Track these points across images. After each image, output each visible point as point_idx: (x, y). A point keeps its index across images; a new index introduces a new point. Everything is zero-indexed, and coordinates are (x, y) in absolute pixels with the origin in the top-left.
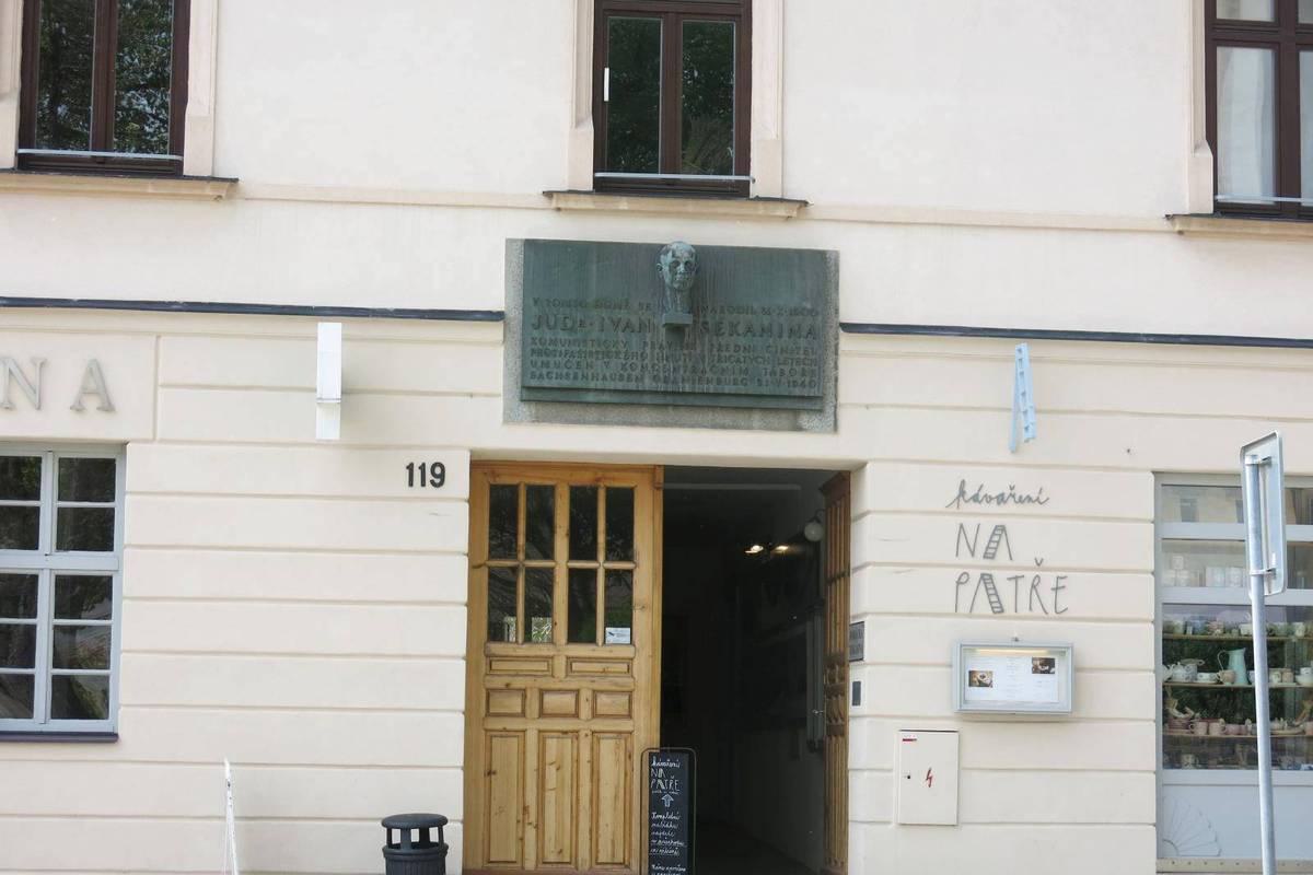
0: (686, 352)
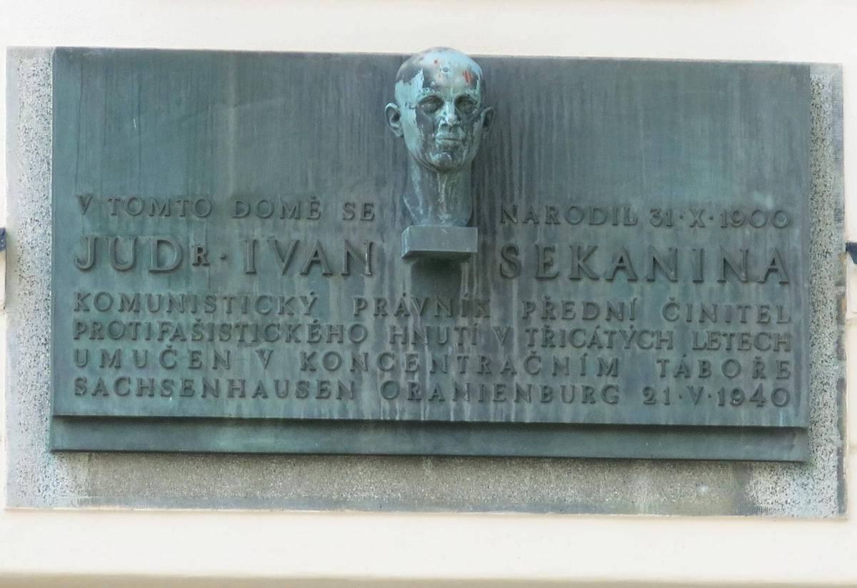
0: (463, 322)
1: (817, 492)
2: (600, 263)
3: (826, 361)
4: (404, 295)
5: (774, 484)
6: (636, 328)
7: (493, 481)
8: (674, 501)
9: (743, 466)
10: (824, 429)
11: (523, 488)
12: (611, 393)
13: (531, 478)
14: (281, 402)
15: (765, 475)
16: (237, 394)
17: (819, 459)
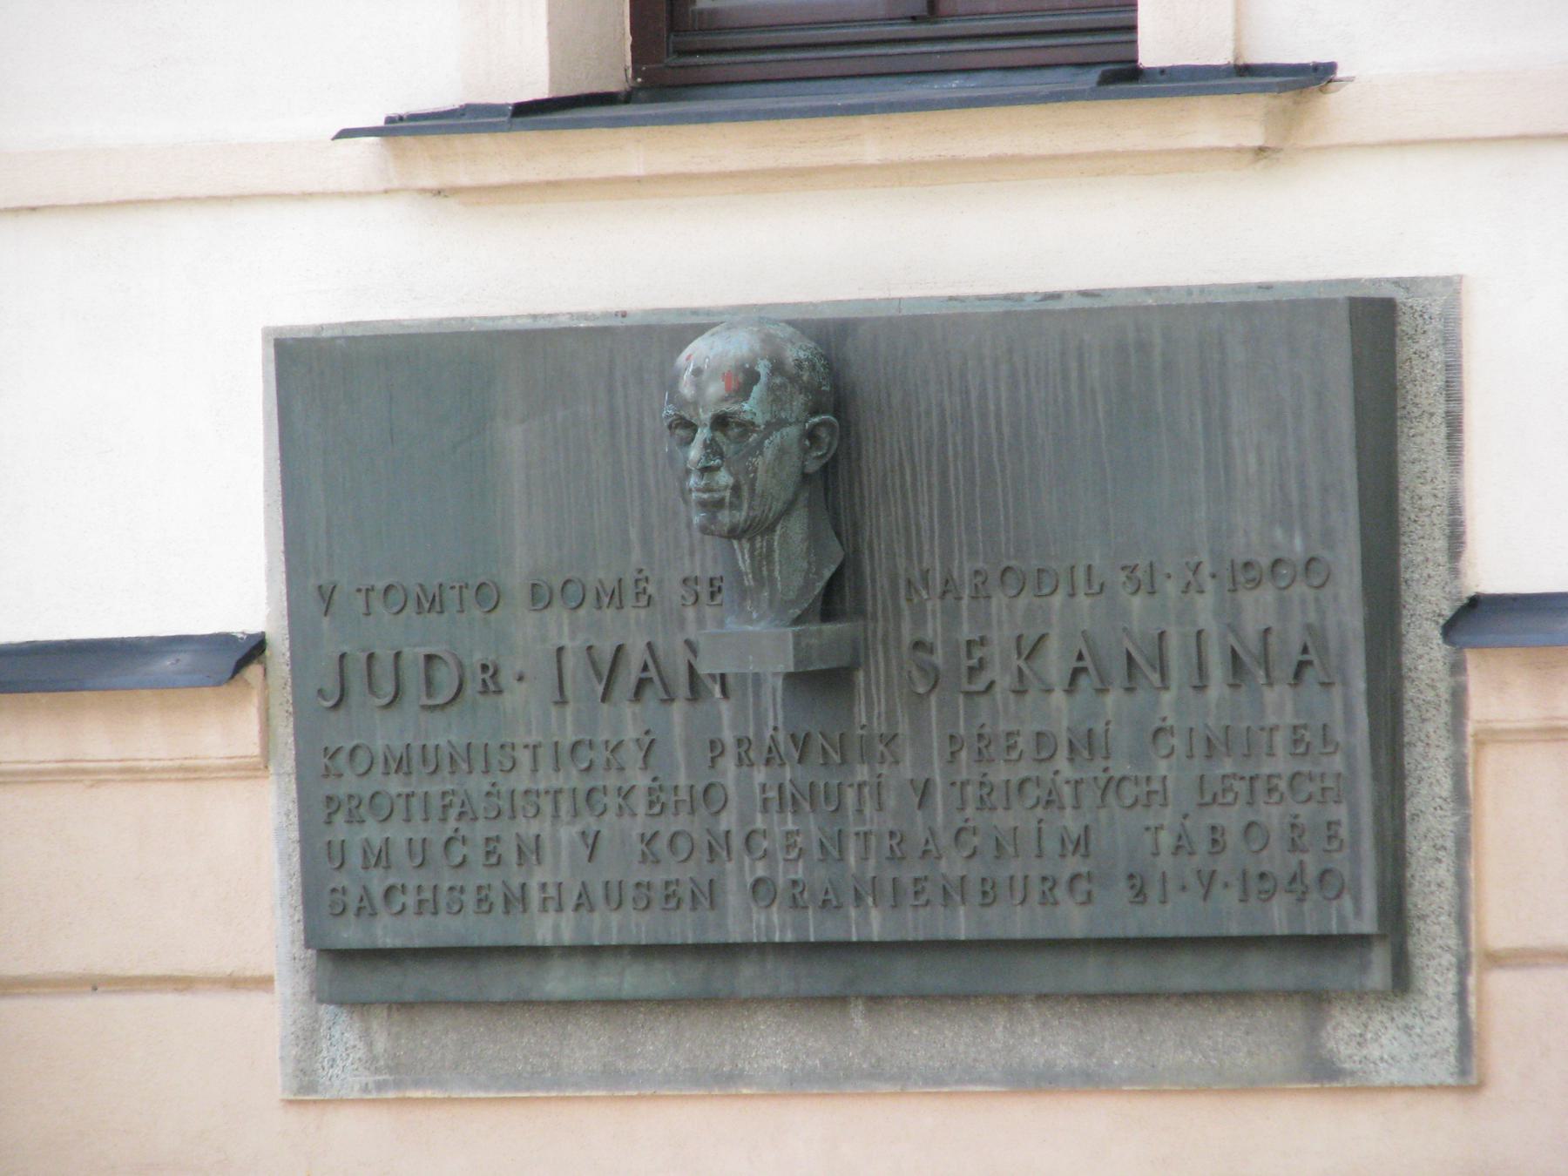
0: (862, 773)
1: (1429, 1039)
2: (1054, 663)
3: (1441, 809)
4: (775, 729)
5: (1363, 1027)
6: (1112, 773)
7: (951, 1034)
8: (1214, 1062)
9: (1316, 1000)
10: (1437, 928)
11: (993, 1045)
12: (1082, 886)
13: (1005, 1027)
14: (615, 918)
15: (1350, 1012)
16: (551, 905)
17: (1431, 982)
